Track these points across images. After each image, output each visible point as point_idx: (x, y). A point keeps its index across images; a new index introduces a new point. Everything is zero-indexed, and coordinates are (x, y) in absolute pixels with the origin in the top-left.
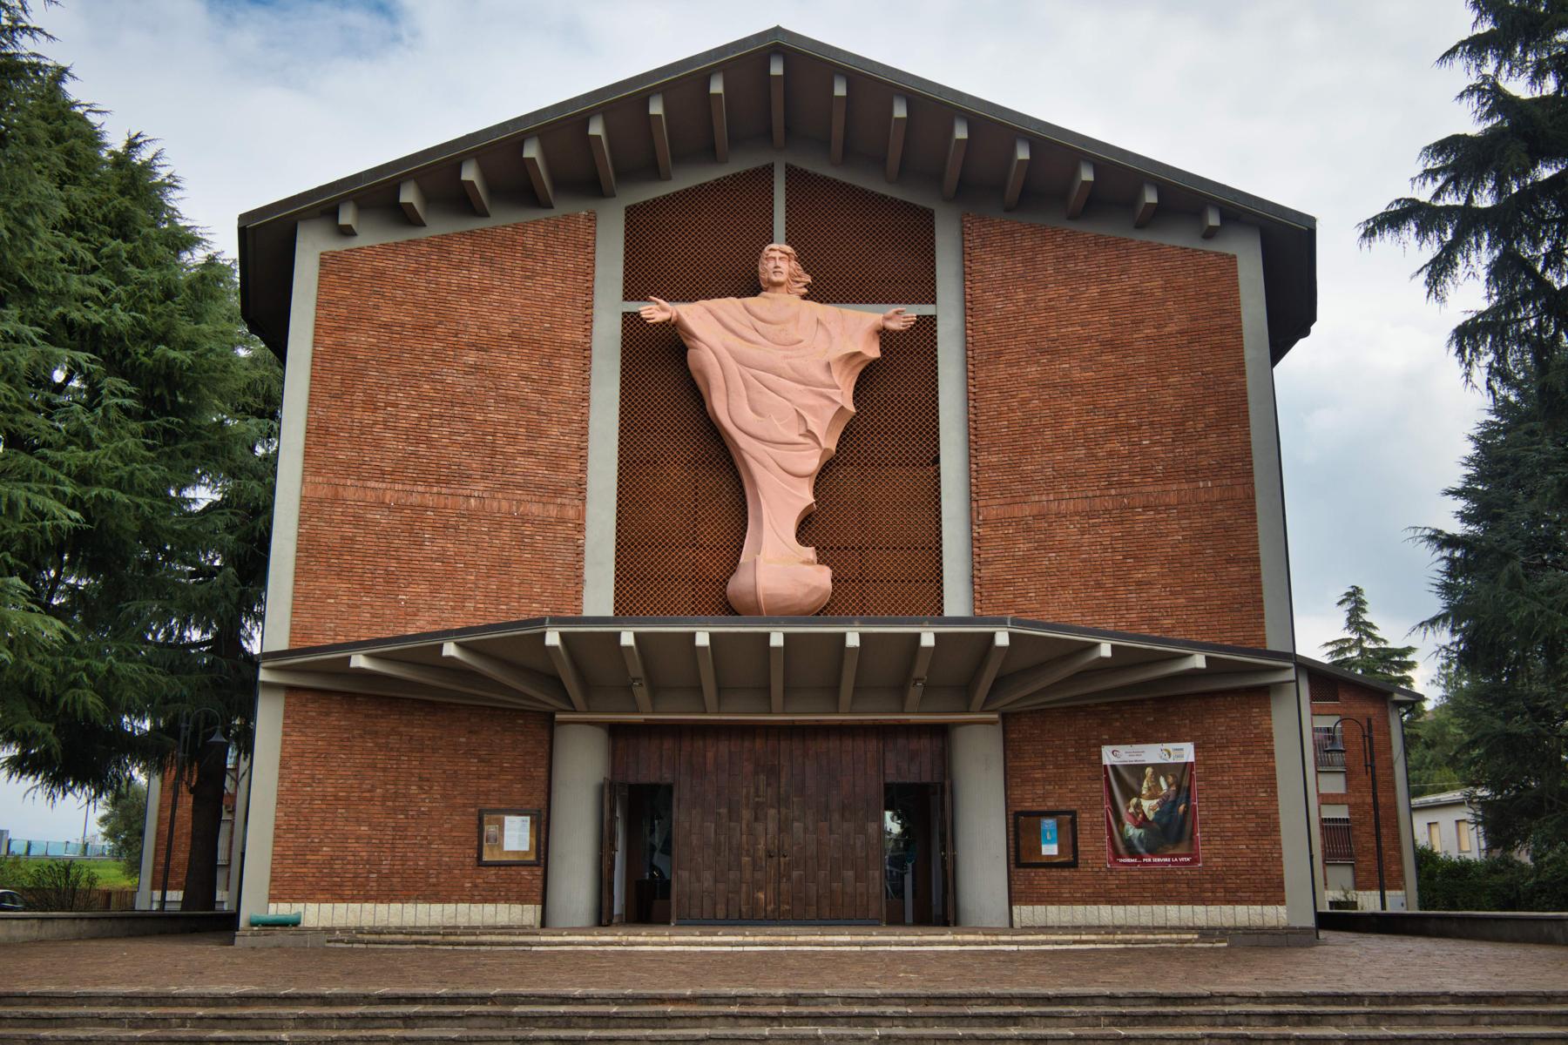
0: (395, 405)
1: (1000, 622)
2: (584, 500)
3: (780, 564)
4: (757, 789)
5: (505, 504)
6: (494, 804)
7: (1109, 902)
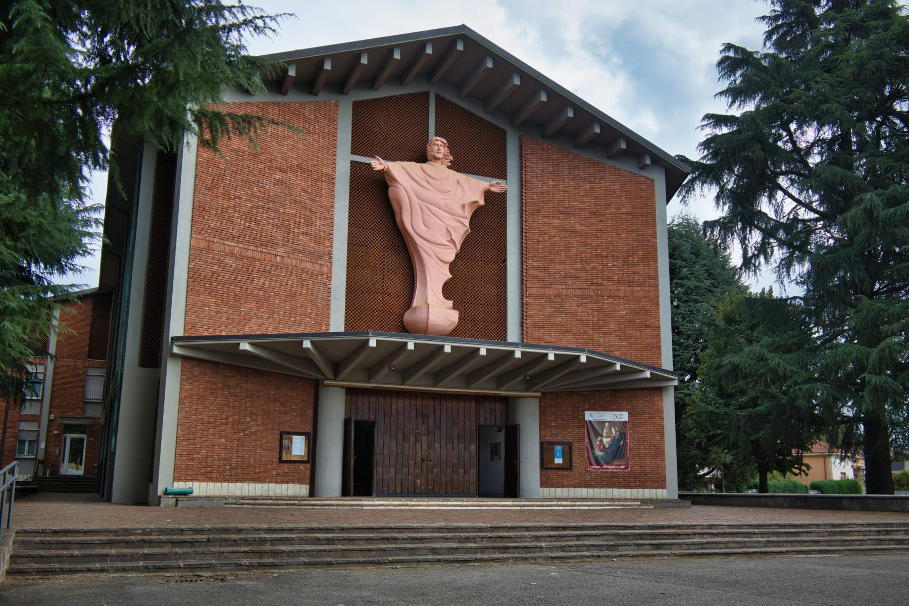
0: (240, 198)
1: (583, 351)
2: (331, 263)
3: (436, 309)
4: (417, 426)
5: (294, 261)
6: (287, 429)
7: (586, 487)
